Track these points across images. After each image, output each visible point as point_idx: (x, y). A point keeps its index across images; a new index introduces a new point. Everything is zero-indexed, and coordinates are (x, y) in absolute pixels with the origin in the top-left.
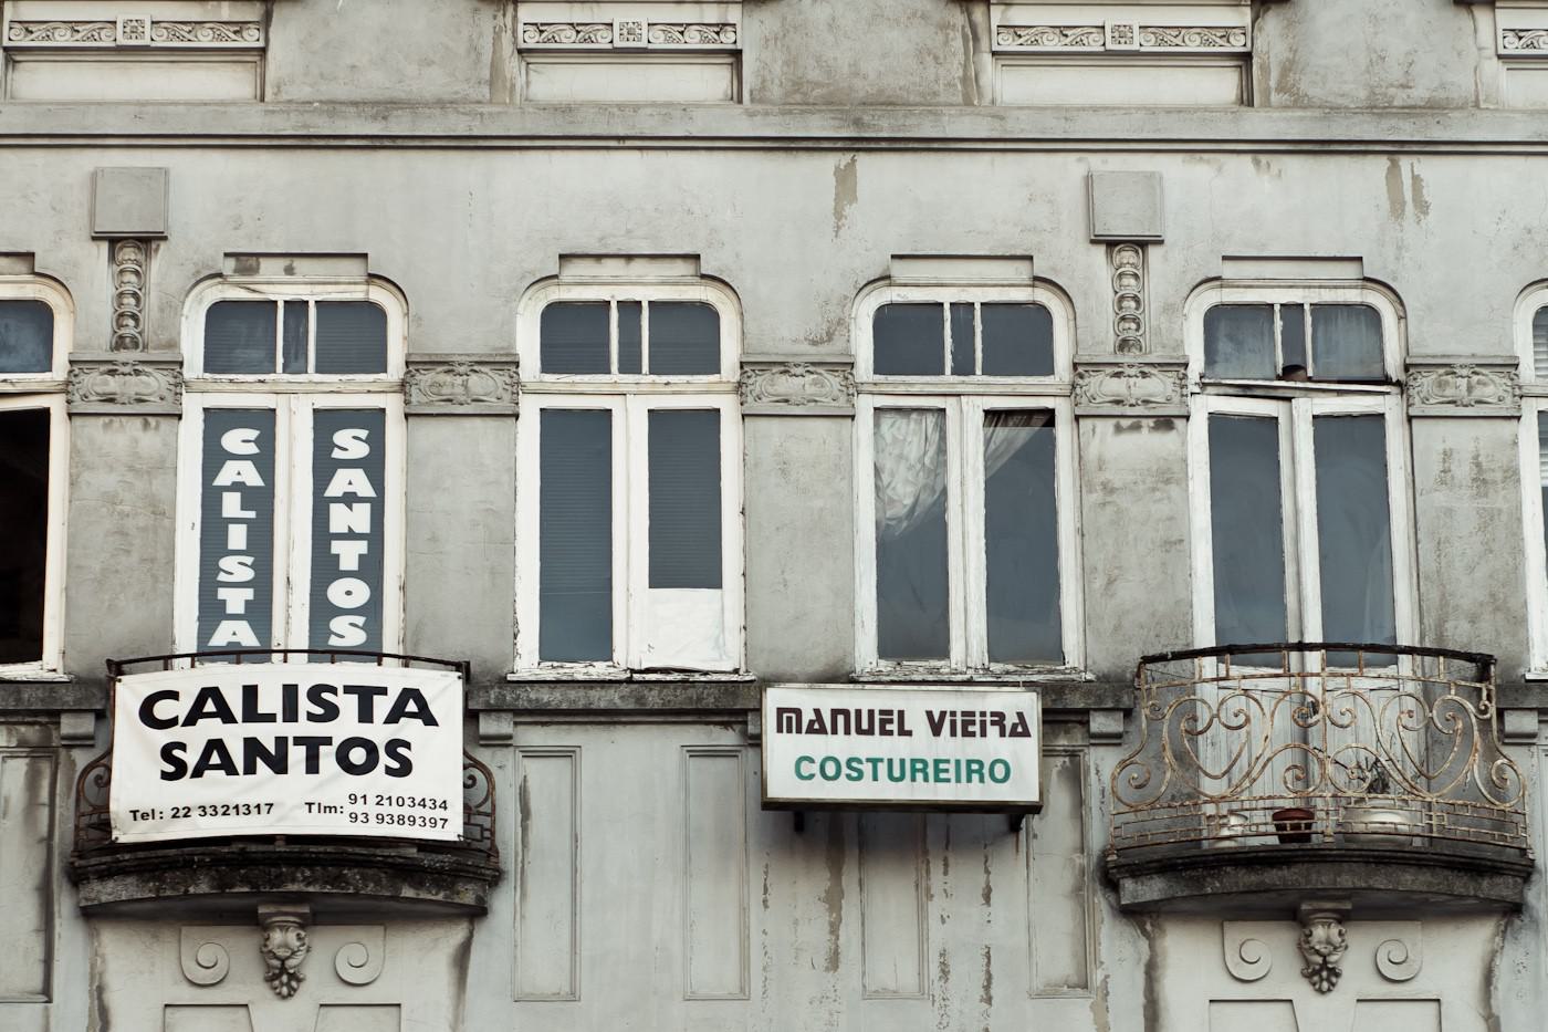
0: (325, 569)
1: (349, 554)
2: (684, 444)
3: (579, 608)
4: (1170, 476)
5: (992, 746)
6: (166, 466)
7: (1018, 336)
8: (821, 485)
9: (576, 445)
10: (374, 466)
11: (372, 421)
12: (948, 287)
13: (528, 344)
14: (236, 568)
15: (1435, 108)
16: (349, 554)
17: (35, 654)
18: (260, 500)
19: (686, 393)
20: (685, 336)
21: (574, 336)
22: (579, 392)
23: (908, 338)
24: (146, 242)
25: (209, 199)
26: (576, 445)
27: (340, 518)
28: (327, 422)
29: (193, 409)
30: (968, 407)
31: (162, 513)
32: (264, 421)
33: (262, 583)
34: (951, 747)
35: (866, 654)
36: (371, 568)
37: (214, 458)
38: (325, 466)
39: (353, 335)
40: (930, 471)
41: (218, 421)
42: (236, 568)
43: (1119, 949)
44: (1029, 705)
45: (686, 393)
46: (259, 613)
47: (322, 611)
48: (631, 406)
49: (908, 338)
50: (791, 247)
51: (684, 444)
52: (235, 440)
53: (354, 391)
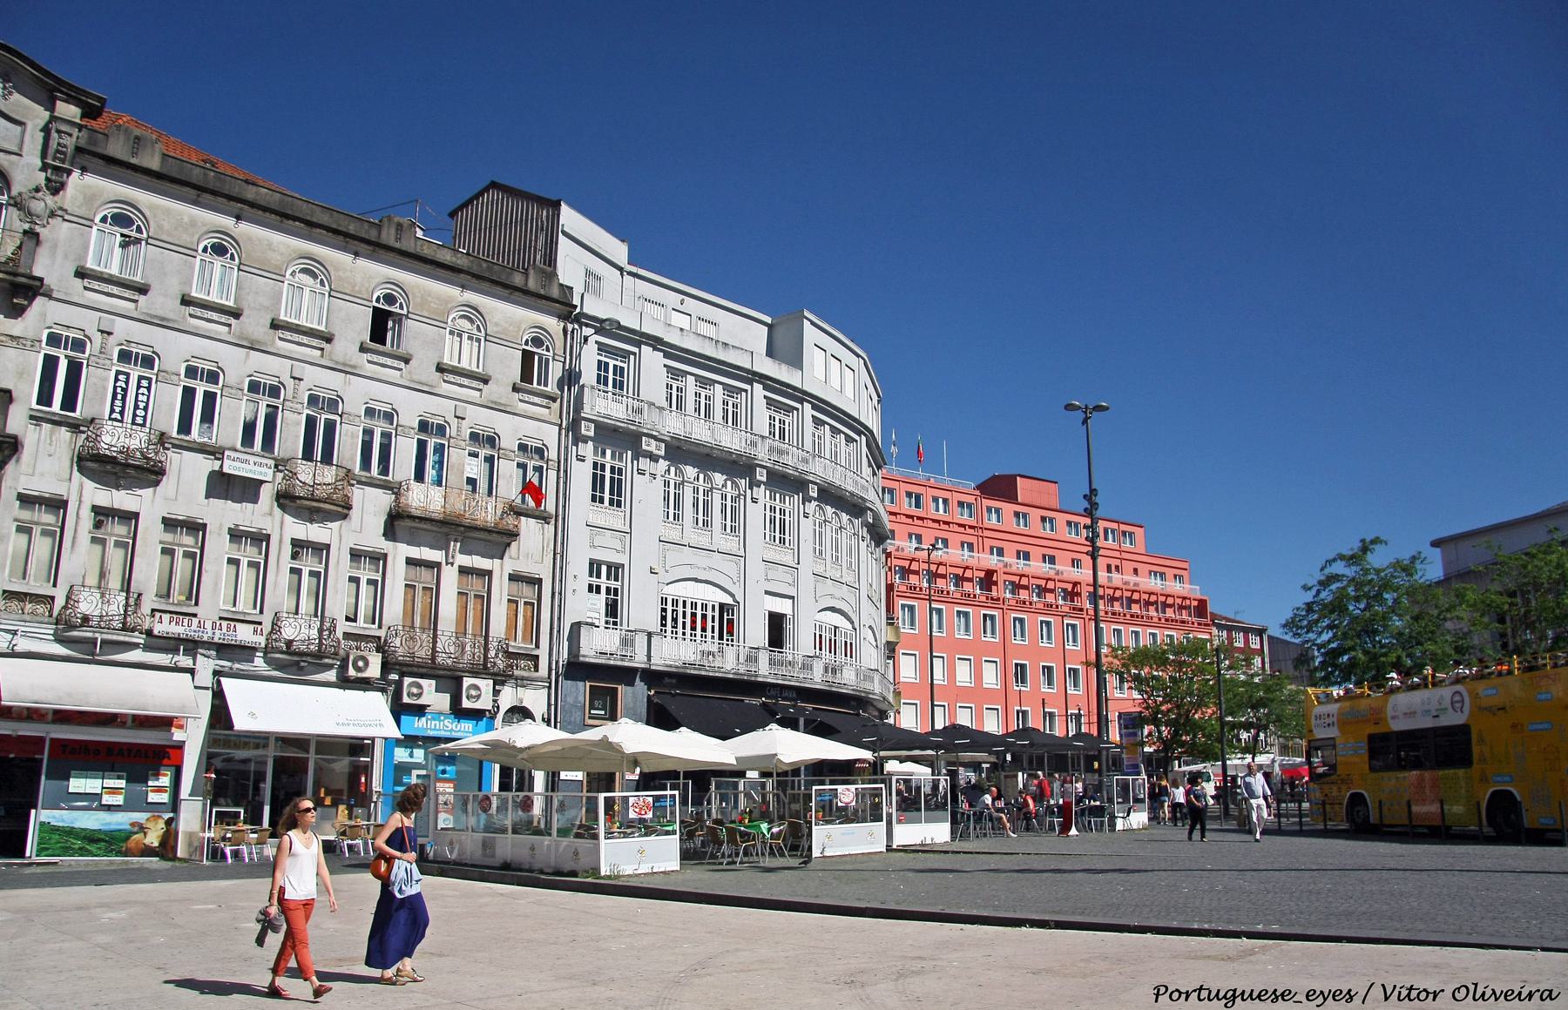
0: (136, 407)
1: (142, 405)
2: (210, 398)
3: (185, 426)
4: (299, 424)
5: (264, 469)
6: (106, 379)
7: (274, 391)
8: (234, 412)
9: (189, 393)
10: (149, 389)
11: (150, 380)
12: (200, 365)
13: (183, 372)
14: (118, 403)
15: (354, 367)
16: (142, 405)
17: (74, 410)
18: (125, 390)
19: (211, 388)
20: (213, 377)
21: (192, 372)
22: (191, 383)
23: (254, 387)
24: (109, 334)
25: (123, 329)
26: (189, 393)
27: (141, 397)
28: (140, 378)
29: (114, 369)
30: (263, 403)
31: (105, 389)
32: (128, 375)
33: (123, 407)
34: (257, 468)
35: (239, 446)
36: (146, 409)
37: (117, 380)
38: (139, 387)
39: (148, 362)
40: (1164, 742)
41: (118, 373)
42: (118, 403)
43: (277, 511)
44: (272, 463)
45: (211, 388)
46: (122, 413)
47: (135, 415)
48: (201, 388)
49: (254, 387)
50: (238, 365)
51: (210, 398)
52: (121, 377)
53: (147, 373)
